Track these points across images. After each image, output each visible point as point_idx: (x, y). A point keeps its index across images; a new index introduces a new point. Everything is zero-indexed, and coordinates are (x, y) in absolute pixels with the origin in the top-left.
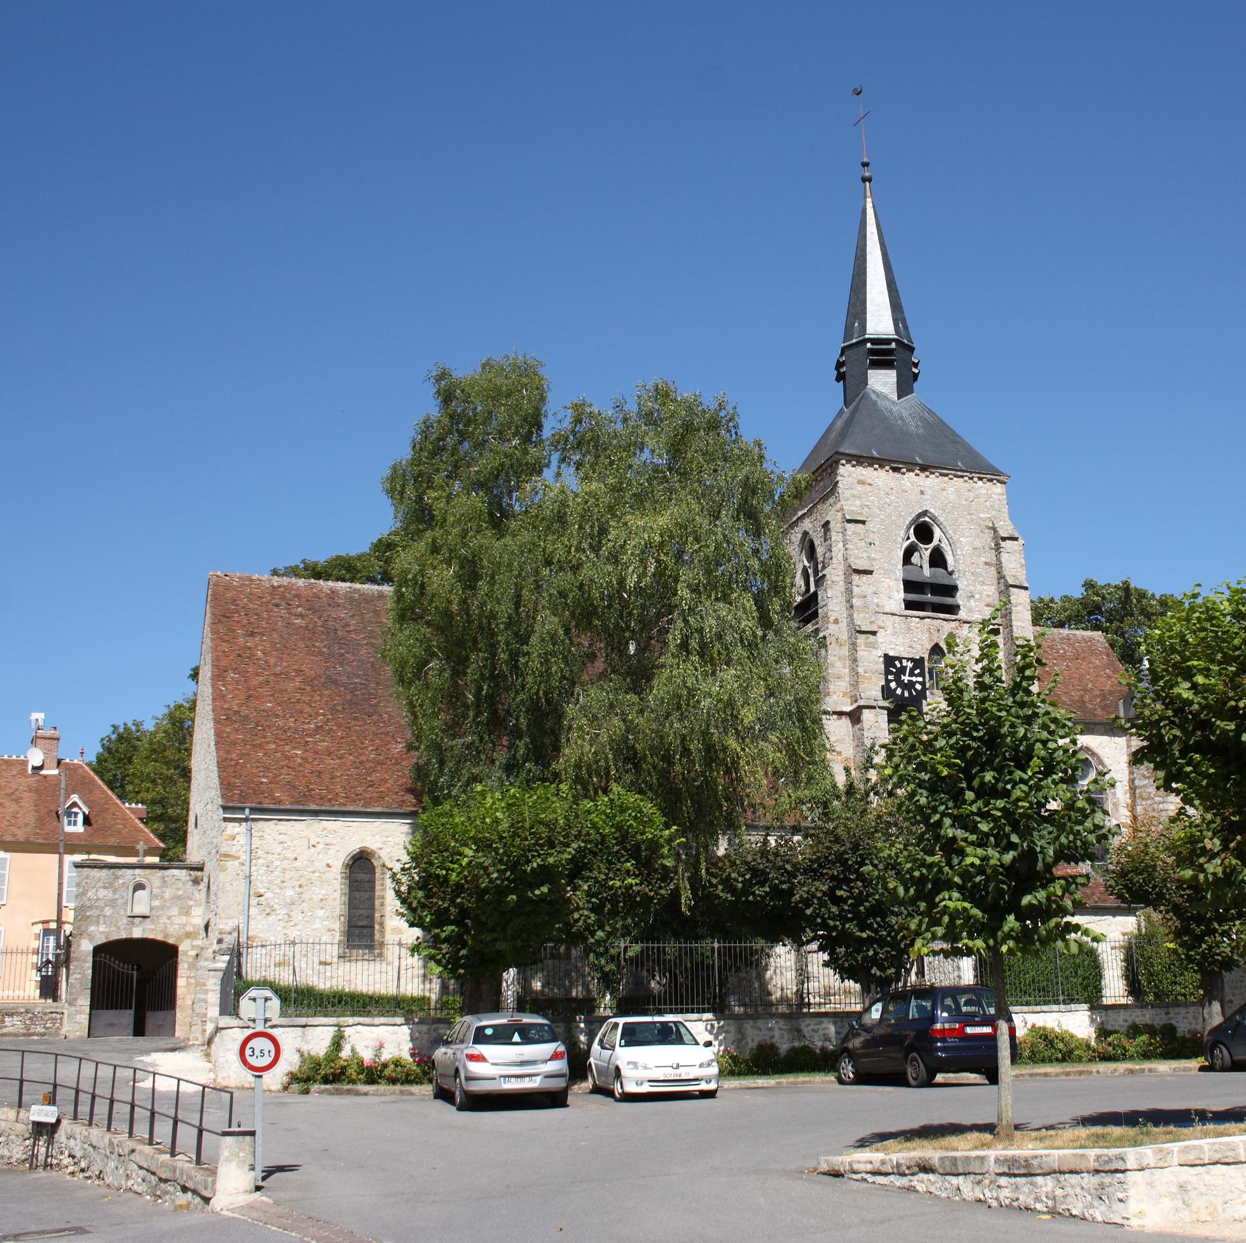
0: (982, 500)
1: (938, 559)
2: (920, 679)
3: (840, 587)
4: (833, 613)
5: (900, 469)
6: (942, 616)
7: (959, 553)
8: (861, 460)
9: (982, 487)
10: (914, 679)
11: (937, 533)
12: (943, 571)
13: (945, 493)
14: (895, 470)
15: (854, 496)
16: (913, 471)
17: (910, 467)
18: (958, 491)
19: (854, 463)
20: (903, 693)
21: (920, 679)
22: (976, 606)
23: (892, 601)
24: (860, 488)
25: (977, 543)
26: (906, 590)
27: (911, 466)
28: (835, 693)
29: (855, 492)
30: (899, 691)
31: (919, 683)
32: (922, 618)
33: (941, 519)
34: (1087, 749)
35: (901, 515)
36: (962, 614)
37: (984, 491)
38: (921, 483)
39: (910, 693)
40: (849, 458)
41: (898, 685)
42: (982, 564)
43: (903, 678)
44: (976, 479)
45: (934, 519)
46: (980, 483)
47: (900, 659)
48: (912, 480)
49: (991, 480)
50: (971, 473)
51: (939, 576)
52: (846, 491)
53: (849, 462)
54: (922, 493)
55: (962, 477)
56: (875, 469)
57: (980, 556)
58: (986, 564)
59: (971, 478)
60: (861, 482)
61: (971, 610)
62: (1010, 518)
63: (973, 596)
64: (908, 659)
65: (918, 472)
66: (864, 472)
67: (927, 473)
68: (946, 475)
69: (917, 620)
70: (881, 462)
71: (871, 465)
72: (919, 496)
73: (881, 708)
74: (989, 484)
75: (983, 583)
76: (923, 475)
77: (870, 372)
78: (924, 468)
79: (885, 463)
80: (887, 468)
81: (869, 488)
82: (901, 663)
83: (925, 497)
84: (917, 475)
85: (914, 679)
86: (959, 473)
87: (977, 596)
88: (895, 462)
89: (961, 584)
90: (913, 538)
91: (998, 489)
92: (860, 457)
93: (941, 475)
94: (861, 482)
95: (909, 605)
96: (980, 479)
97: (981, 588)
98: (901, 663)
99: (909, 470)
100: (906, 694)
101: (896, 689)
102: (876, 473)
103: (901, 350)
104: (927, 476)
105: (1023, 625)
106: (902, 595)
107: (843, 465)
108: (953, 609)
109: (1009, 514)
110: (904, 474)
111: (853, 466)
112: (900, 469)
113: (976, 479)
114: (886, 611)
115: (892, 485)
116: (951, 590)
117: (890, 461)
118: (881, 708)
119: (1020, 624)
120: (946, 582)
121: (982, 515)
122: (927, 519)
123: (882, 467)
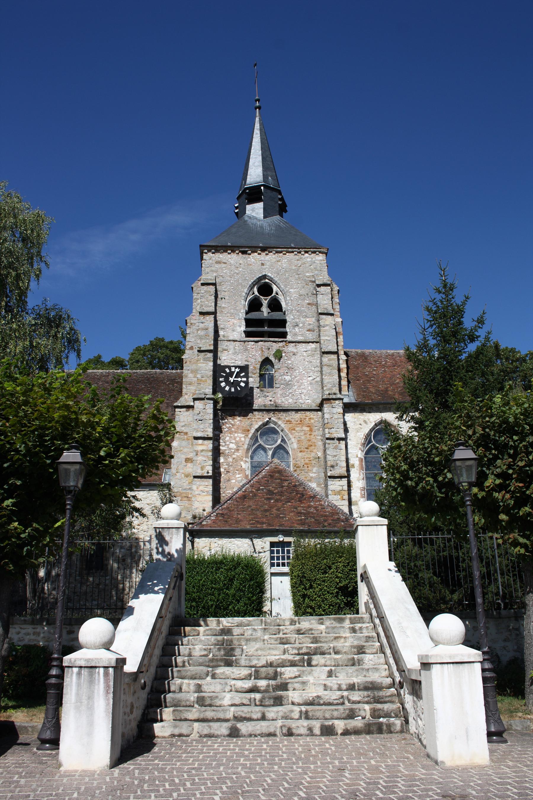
0: (307, 265)
1: (275, 305)
2: (245, 379)
3: (340, 348)
4: (190, 343)
5: (247, 251)
6: (276, 339)
7: (288, 299)
8: (218, 249)
9: (308, 257)
10: (239, 379)
11: (275, 288)
12: (280, 313)
13: (279, 263)
14: (244, 253)
15: (212, 271)
16: (256, 252)
17: (254, 249)
18: (290, 261)
19: (214, 251)
20: (230, 389)
21: (245, 379)
22: (300, 331)
23: (235, 333)
24: (217, 266)
25: (303, 292)
26: (247, 326)
27: (254, 249)
28: (186, 394)
29: (213, 269)
30: (227, 388)
31: (244, 382)
32: (257, 342)
33: (276, 279)
34: (275, 423)
35: (245, 280)
36: (289, 338)
37: (309, 260)
38: (263, 259)
39: (236, 389)
40: (210, 248)
41: (227, 385)
42: (306, 304)
43: (230, 379)
44: (303, 253)
45: (271, 279)
46: (307, 255)
47: (229, 367)
48: (255, 258)
49: (314, 252)
50: (299, 249)
51: (276, 315)
52: (207, 269)
53: (209, 251)
54: (263, 264)
55: (293, 252)
56: (229, 254)
57: (304, 299)
58: (309, 304)
59: (300, 252)
60: (218, 262)
61: (295, 334)
62: (328, 275)
63: (297, 325)
64: (236, 367)
65: (259, 252)
66: (221, 256)
67: (267, 252)
68: (281, 252)
69: (253, 343)
70: (232, 249)
71: (225, 251)
72: (260, 267)
73: (208, 399)
74: (313, 255)
75: (306, 317)
76: (263, 254)
77: (247, 206)
78: (263, 249)
79: (235, 249)
80: (237, 252)
81: (224, 265)
82: (230, 369)
83: (265, 267)
84: (259, 254)
85: (239, 379)
86: (290, 250)
87: (301, 325)
88: (242, 247)
89: (289, 318)
90: (256, 293)
91: (321, 257)
92: (217, 246)
93: (277, 252)
94: (218, 262)
95: (248, 334)
96: (306, 252)
97: (304, 319)
98: (230, 369)
99: (253, 252)
100: (233, 390)
101: (225, 387)
102: (229, 256)
103: (269, 191)
104: (267, 254)
105: (329, 338)
106: (243, 328)
107: (206, 253)
108: (284, 335)
109: (328, 272)
110: (250, 254)
111: (213, 253)
112: (247, 251)
113: (303, 253)
114: (230, 339)
115: (241, 262)
116: (283, 323)
117: (238, 247)
118: (208, 399)
119: (327, 338)
120: (282, 318)
121: (307, 274)
122: (267, 281)
123: (233, 251)
